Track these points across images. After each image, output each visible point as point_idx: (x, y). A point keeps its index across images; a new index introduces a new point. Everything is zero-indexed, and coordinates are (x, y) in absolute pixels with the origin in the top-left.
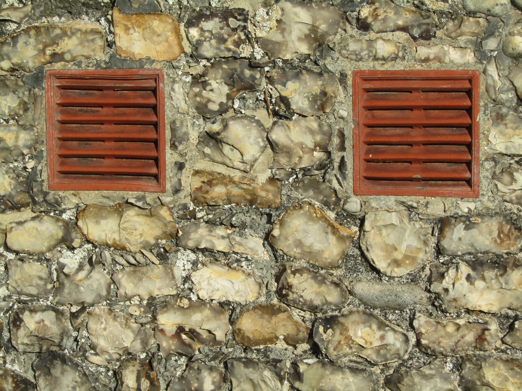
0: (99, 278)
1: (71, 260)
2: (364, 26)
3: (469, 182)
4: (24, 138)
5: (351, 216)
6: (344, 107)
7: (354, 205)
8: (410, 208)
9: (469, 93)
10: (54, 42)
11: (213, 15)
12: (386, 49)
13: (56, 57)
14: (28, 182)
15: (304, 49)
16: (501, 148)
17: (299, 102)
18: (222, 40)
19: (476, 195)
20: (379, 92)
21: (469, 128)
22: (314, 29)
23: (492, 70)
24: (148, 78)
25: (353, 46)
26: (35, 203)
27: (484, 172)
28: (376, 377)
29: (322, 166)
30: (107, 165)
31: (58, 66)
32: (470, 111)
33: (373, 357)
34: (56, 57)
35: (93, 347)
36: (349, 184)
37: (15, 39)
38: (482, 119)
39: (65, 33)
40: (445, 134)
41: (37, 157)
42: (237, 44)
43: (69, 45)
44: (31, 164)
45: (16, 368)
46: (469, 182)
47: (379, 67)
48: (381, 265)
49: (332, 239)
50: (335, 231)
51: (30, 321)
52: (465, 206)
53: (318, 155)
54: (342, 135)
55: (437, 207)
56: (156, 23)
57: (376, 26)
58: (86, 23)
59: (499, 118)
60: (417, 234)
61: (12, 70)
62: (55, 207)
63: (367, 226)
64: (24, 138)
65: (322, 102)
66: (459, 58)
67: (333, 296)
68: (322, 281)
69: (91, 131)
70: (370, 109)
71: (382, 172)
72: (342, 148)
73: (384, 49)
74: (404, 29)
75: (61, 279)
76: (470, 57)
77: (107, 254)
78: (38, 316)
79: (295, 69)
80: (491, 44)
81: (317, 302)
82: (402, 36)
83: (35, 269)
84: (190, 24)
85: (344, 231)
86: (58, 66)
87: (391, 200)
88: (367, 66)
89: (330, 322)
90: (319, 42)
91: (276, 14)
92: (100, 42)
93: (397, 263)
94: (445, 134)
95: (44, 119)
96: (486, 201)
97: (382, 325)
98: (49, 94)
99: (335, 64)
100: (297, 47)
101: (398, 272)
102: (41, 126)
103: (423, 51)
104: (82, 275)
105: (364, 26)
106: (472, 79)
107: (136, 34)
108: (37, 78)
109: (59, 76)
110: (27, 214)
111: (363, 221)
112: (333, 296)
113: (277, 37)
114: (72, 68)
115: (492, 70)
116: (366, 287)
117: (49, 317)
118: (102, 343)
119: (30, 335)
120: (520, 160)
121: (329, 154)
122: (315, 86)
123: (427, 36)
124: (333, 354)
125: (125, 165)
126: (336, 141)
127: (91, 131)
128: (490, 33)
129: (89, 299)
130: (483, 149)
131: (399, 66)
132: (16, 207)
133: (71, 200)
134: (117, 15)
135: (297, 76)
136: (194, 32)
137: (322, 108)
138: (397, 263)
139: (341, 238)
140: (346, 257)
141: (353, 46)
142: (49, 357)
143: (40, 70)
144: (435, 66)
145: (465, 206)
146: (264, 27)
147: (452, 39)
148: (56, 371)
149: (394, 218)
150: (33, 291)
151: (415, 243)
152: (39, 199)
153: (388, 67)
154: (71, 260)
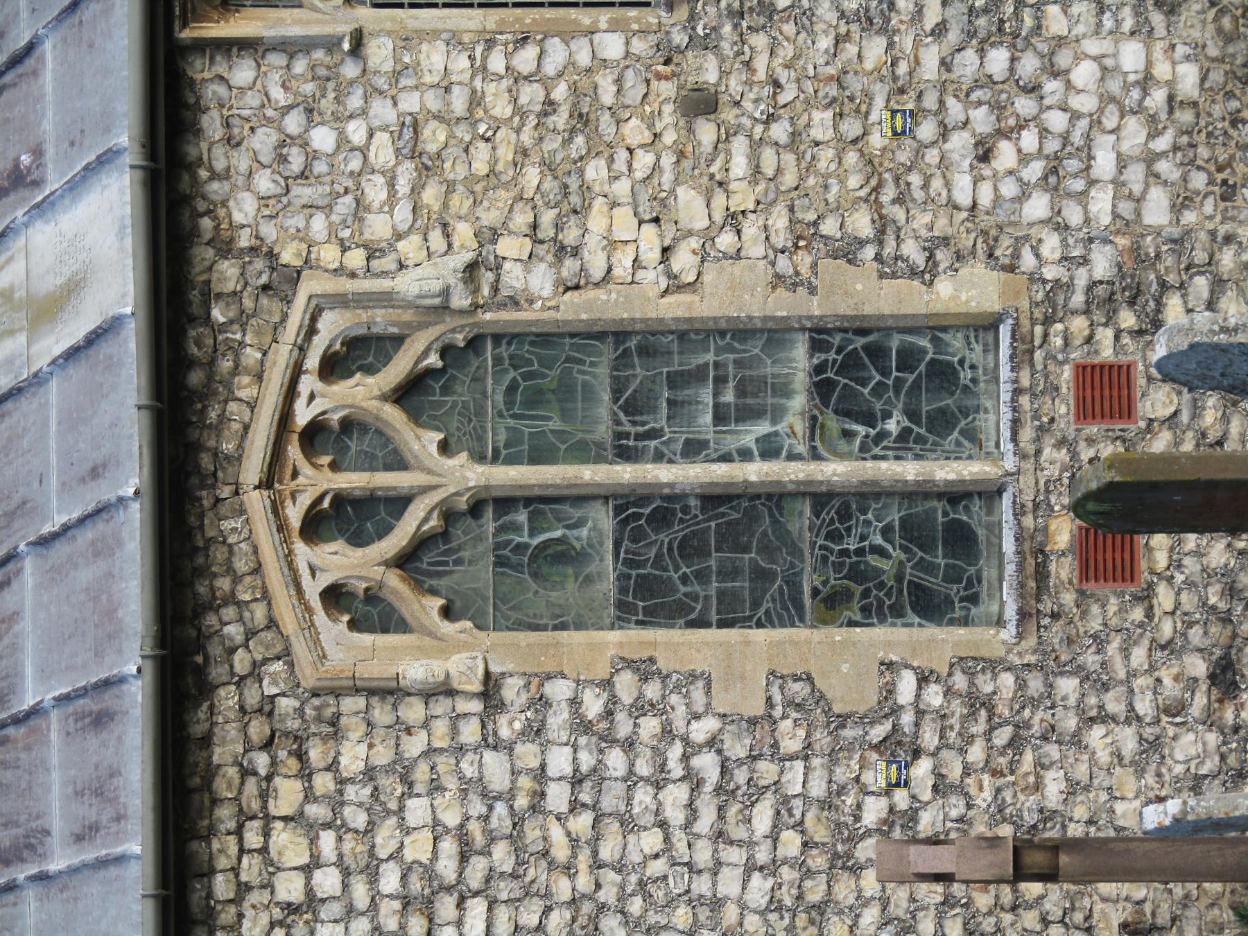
0: (1187, 561)
1: (1180, 578)
2: (1052, 420)
3: (1129, 367)
4: (1113, 600)
5: (1149, 426)
6: (1093, 429)
7: (1142, 424)
8: (1143, 395)
9: (1084, 368)
10: (1063, 583)
11: (1048, 498)
12: (1064, 409)
13: (1070, 582)
14: (1136, 599)
15: (1064, 451)
16: (1111, 351)
17: (1091, 453)
18: (1060, 494)
19: (1135, 362)
20: (1085, 412)
21: (1102, 367)
22: (1054, 446)
23: (1073, 356)
24: (1081, 535)
25: (1062, 426)
26: (1148, 596)
27: (1123, 359)
28: (653, 39)
29: (1124, 441)
30: (1127, 556)
31: (1075, 581)
32: (1093, 367)
33: (1220, 413)
34: (1070, 582)
35: (1226, 566)
36: (1132, 427)
37: (1062, 605)
38: (1096, 361)
39: (1058, 577)
40: (1106, 379)
41: (1123, 594)
42: (1062, 485)
43: (1064, 574)
44: (1127, 597)
45: (1240, 609)
46: (1129, 367)
47: (1072, 412)
48: (1172, 409)
49: (1160, 435)
50: (1157, 434)
51: (1213, 600)
52: (1141, 367)
53: (1118, 443)
54: (1107, 431)
55: (1141, 381)
56: (1052, 528)
57: (1052, 414)
58: (1053, 567)
59: (1097, 352)
60: (1156, 392)
61: (1078, 606)
62: (1151, 586)
63: (1153, 417)
64: (1113, 600)
65: (1091, 441)
66: (1067, 373)
67: (1190, 434)
68: (1183, 440)
69: (1110, 564)
70: (1094, 417)
71: (1126, 410)
72: (1113, 430)
73: (1063, 410)
74: (1053, 400)
75: (1190, 584)
76: (1067, 367)
77: (1175, 557)
78: (1210, 596)
79: (1074, 455)
80: (1060, 357)
81: (1194, 442)
82: (1057, 401)
83: (1184, 597)
84: (1052, 511)
85: (1157, 429)
86: (1075, 581)
87: (1139, 405)
88: (1072, 418)
89: (1204, 435)
90: (1061, 443)
91: (1047, 465)
92: (1063, 559)
93: (1171, 402)
94: (1106, 379)
95: (1101, 589)
96: (1138, 357)
97: (1204, 409)
98: (1090, 587)
99: (1071, 434)
100: (1063, 455)
101: (1176, 401)
102: (1107, 591)
103: (1064, 390)
104: (1186, 571)
105: (1052, 420)
106: (1077, 367)
107: (1058, 539)
108: (1081, 593)
109: (1081, 581)
110: (1155, 602)
111: (1151, 420)
112: (1190, 434)
113: (1058, 465)
114: (1076, 573)
115: (1073, 356)
116: (1185, 417)
117: (1210, 590)
118: (1223, 560)
119: (1221, 599)
120: (1158, 4)
121: (1117, 438)
122: (1082, 445)
123: (1057, 389)
124: (1220, 434)
125: (1127, 546)
126: (1110, 434)
127: (1110, 564)
128: (1055, 358)
129: (1199, 567)
130: (1112, 359)
131: (1072, 402)
132: (1151, 607)
133: (1146, 575)
134: (1048, 548)
135: (1078, 454)
136: (1057, 508)
137: (1093, 441)
138: (1171, 402)
139: (1160, 431)
140: (1170, 428)
141: (1062, 426)
142: (1231, 591)
143: (1077, 591)
144: (1071, 384)
145: (1141, 367)
146: (1054, 471)
147: (1059, 376)
148: (1240, 586)
149: (1148, 404)
150: (1196, 598)
151: (1161, 393)
152: (1146, 593)
153: (1072, 408)
154: (1180, 578)
